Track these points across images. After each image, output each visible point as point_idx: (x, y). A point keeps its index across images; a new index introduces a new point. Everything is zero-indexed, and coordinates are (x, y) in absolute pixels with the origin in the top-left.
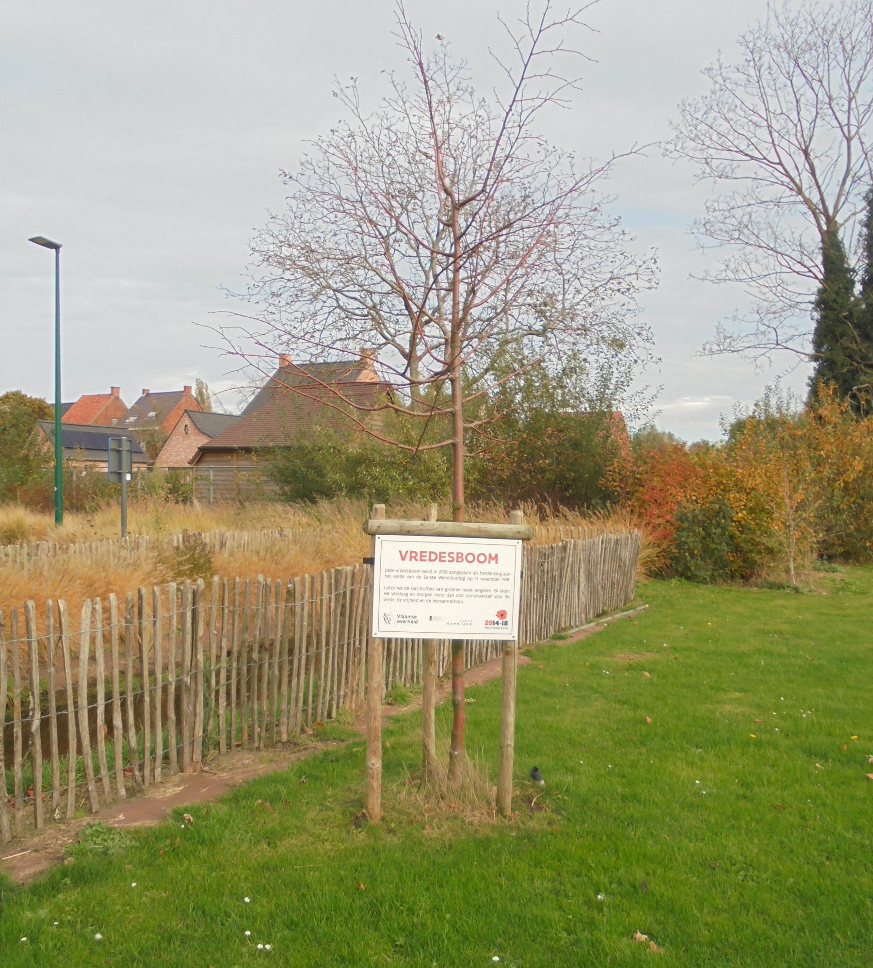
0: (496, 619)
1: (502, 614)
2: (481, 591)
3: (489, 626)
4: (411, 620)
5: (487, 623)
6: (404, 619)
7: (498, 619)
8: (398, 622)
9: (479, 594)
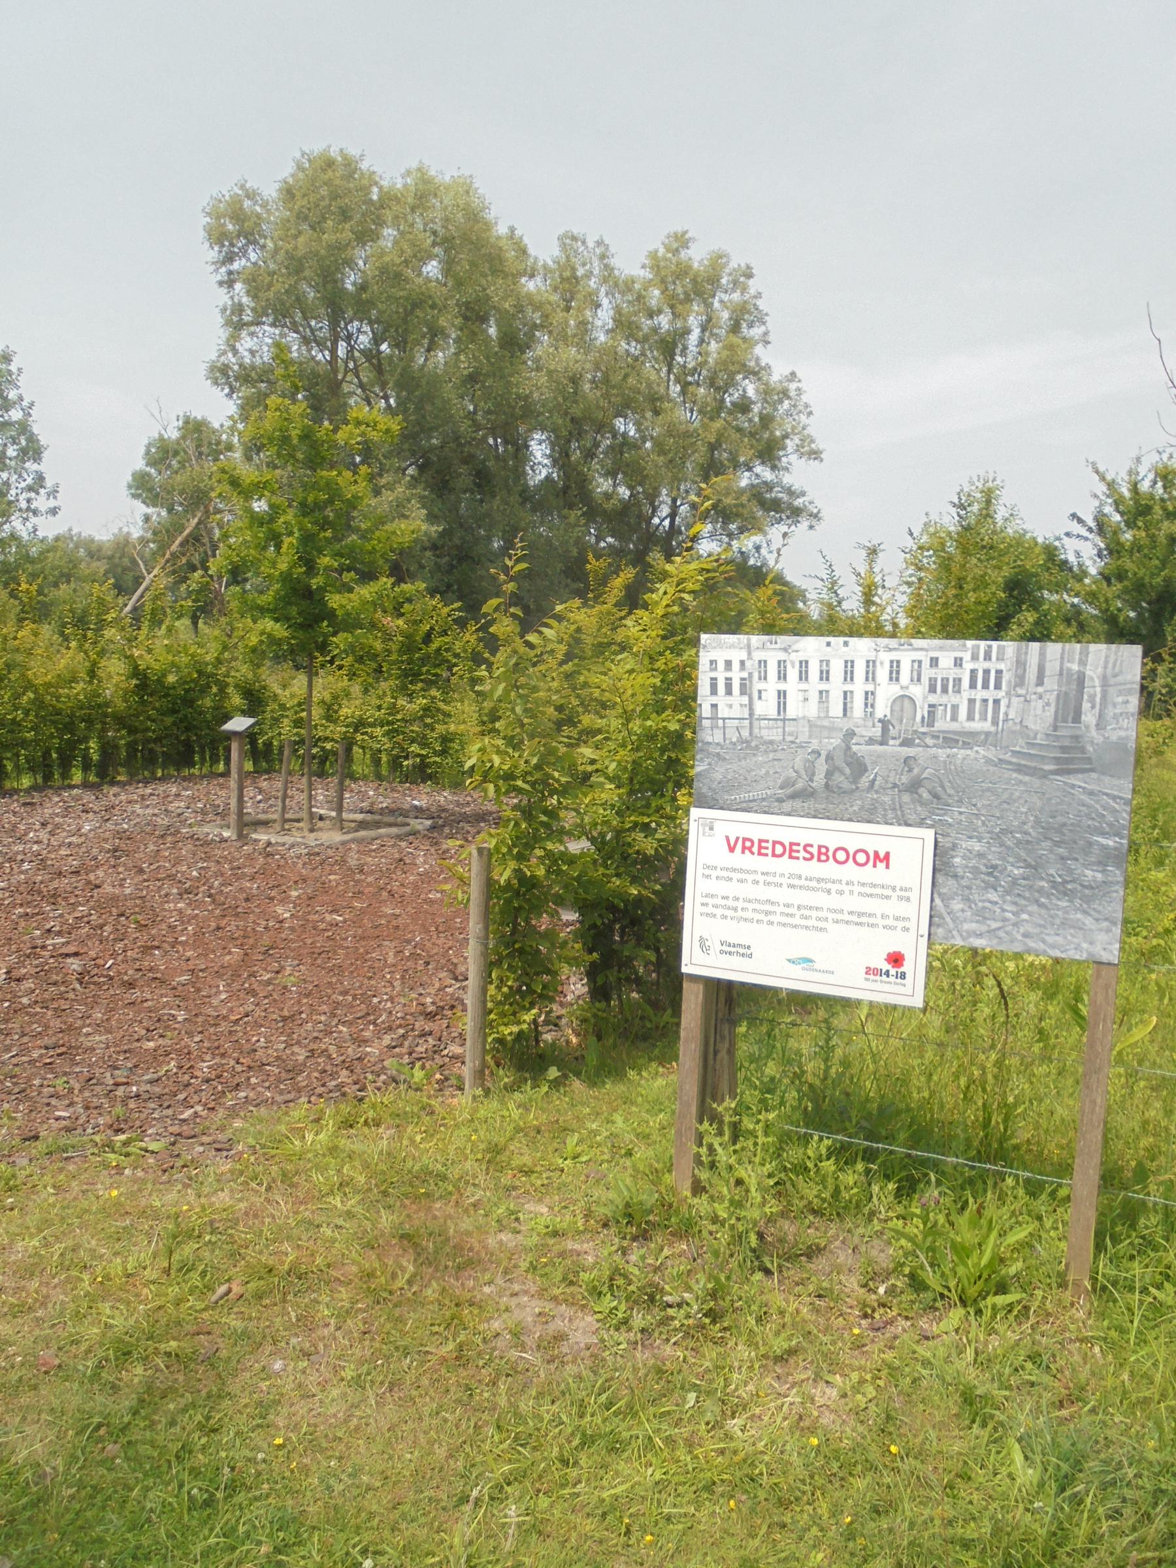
0: (886, 966)
1: (896, 959)
2: (860, 914)
3: (872, 977)
4: (741, 951)
5: (868, 971)
6: (732, 949)
7: (889, 967)
8: (722, 952)
9: (855, 918)
